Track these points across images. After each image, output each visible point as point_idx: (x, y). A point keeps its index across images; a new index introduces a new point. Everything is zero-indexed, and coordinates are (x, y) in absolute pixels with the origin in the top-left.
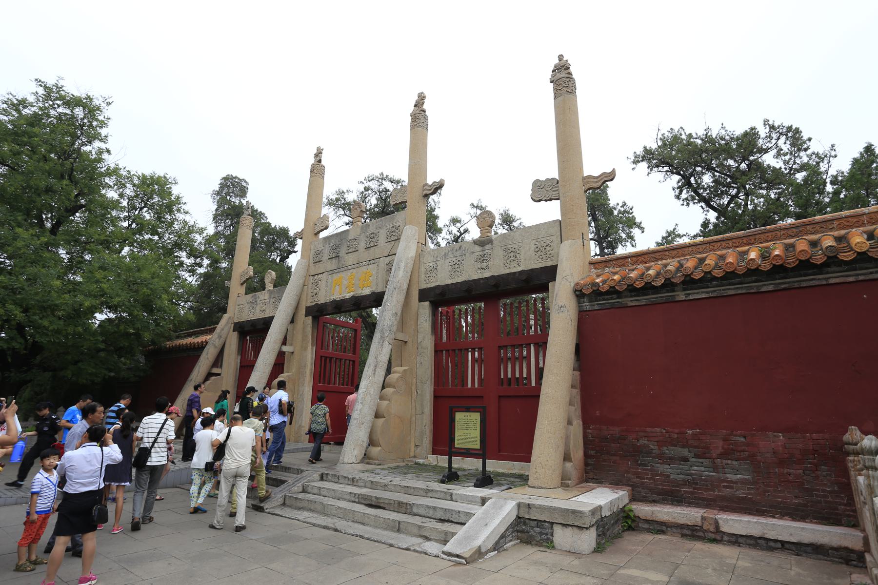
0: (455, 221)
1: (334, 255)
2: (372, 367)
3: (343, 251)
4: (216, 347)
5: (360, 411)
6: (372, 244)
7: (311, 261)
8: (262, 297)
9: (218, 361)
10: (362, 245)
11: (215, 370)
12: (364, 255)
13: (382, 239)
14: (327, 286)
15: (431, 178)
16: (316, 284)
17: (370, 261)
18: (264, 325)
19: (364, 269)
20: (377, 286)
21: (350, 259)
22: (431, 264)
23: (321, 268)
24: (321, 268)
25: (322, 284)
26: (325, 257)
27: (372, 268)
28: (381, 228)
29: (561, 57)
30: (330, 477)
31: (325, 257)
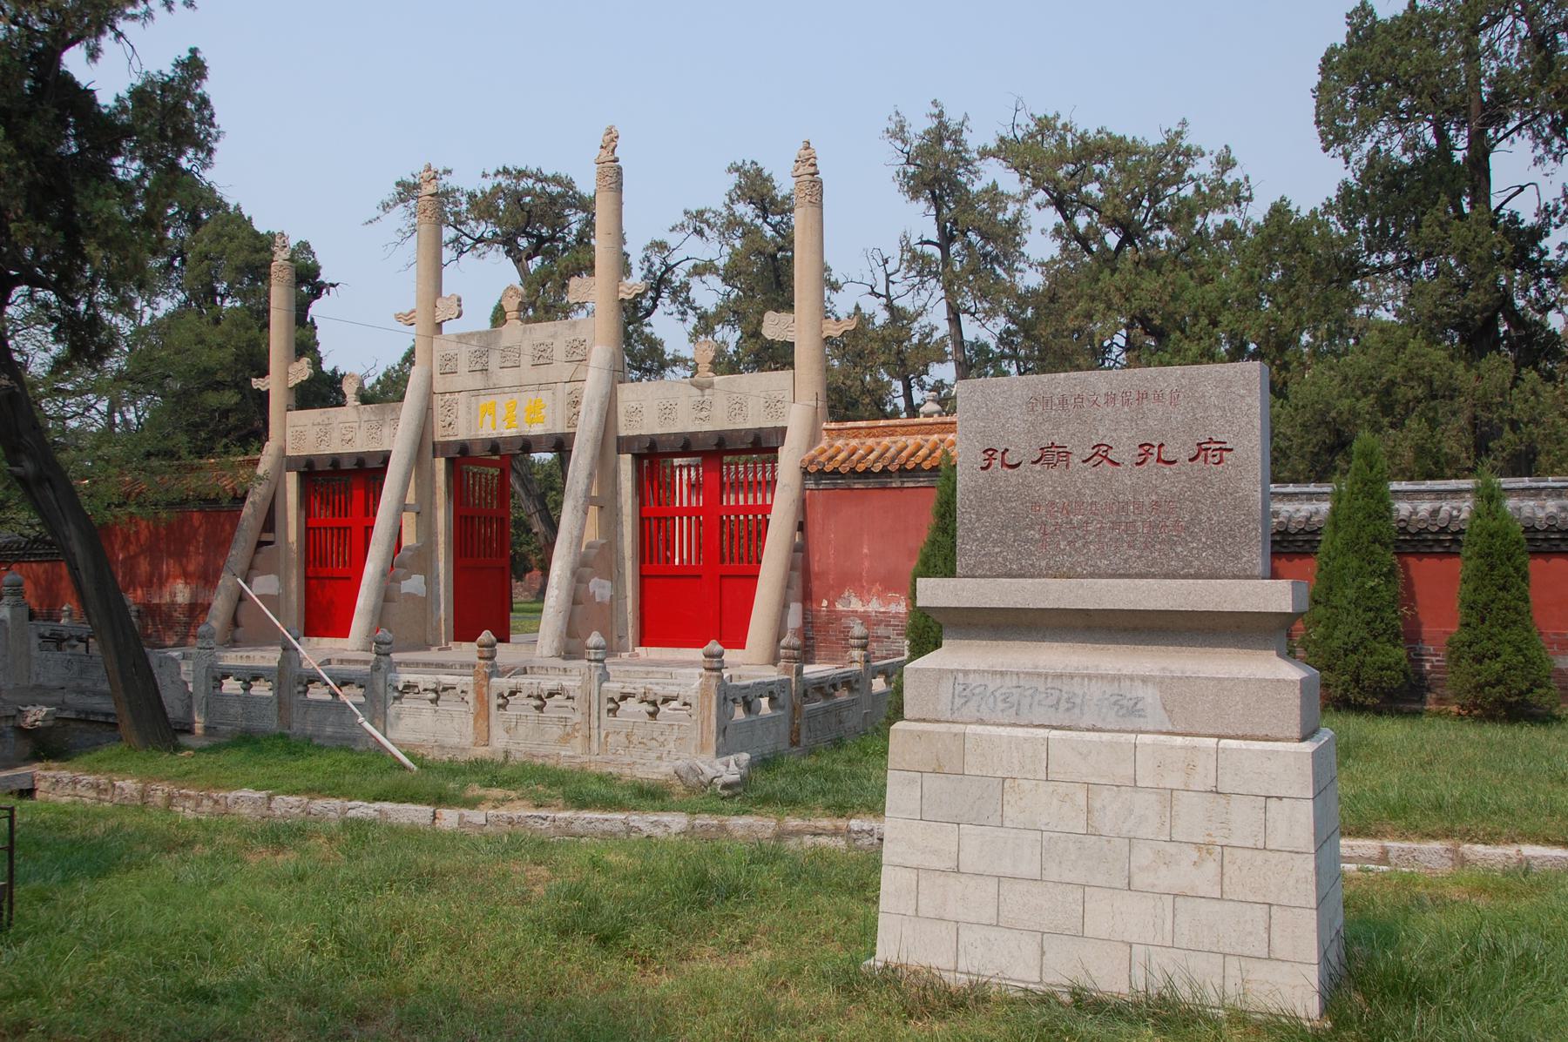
1: (478, 367)
3: (494, 361)
6: (542, 361)
12: (529, 374)
13: (559, 352)
19: (531, 395)
21: (507, 377)
25: (461, 410)
26: (463, 367)
29: (807, 146)
31: (463, 367)
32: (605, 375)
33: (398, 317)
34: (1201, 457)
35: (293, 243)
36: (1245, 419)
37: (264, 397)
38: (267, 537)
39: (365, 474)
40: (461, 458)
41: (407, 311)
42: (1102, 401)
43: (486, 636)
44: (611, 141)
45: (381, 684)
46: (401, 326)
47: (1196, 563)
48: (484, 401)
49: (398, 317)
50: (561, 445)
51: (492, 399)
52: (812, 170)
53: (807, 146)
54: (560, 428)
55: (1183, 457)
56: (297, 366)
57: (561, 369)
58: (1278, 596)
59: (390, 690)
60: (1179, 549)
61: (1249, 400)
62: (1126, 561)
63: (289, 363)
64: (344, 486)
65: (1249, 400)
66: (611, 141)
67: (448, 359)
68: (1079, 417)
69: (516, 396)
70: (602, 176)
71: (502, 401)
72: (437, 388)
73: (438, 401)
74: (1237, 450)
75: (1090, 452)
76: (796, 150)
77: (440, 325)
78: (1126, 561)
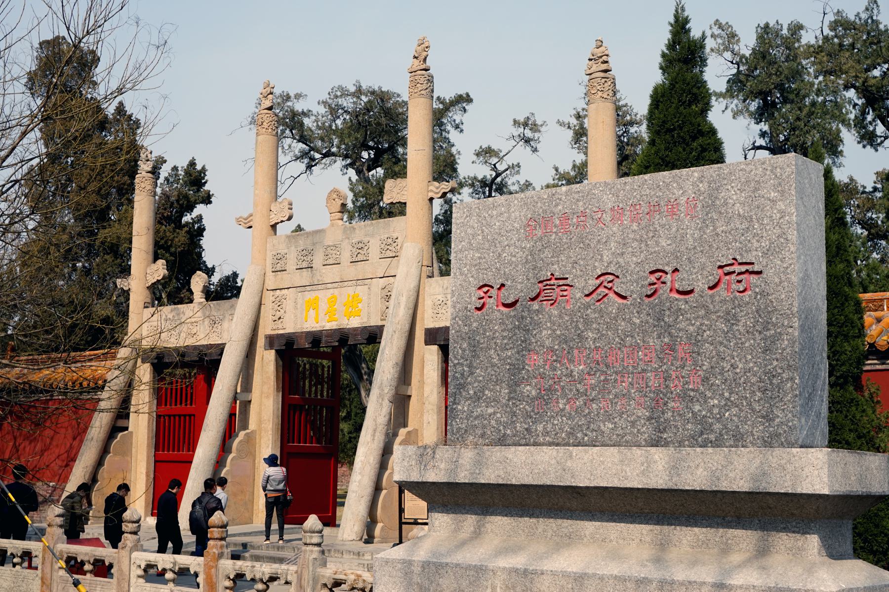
0: (486, 153)
1: (305, 265)
2: (370, 431)
3: (318, 260)
4: (663, 546)
5: (359, 482)
6: (360, 257)
7: (269, 269)
8: (189, 313)
9: (122, 412)
10: (346, 256)
11: (121, 423)
12: (352, 272)
13: (374, 250)
14: (296, 308)
15: (445, 90)
16: (279, 303)
17: (360, 281)
18: (205, 362)
19: (350, 291)
20: (369, 318)
21: (330, 274)
22: (440, 297)
23: (285, 280)
24: (285, 280)
25: (288, 305)
26: (291, 265)
27: (361, 290)
28: (372, 236)
29: (600, 44)
30: (332, 553)
31: (291, 265)
32: (414, 271)
33: (239, 221)
34: (722, 285)
35: (153, 157)
36: (777, 231)
37: (126, 294)
38: (121, 423)
39: (205, 362)
40: (288, 350)
41: (245, 216)
42: (607, 217)
43: (313, 521)
44: (421, 57)
45: (126, 562)
46: (242, 229)
47: (717, 426)
48: (309, 296)
49: (239, 221)
50: (373, 336)
51: (313, 294)
52: (604, 67)
53: (600, 44)
54: (374, 321)
55: (701, 285)
56: (154, 267)
57: (376, 265)
58: (817, 471)
59: (133, 568)
60: (697, 408)
61: (781, 205)
62: (633, 424)
63: (148, 266)
64: (185, 376)
65: (781, 205)
66: (421, 57)
67: (279, 258)
68: (581, 240)
69: (336, 291)
70: (414, 83)
71: (323, 296)
72: (270, 284)
73: (269, 297)
74: (769, 273)
75: (593, 283)
76: (589, 49)
77: (274, 227)
78: (633, 424)
